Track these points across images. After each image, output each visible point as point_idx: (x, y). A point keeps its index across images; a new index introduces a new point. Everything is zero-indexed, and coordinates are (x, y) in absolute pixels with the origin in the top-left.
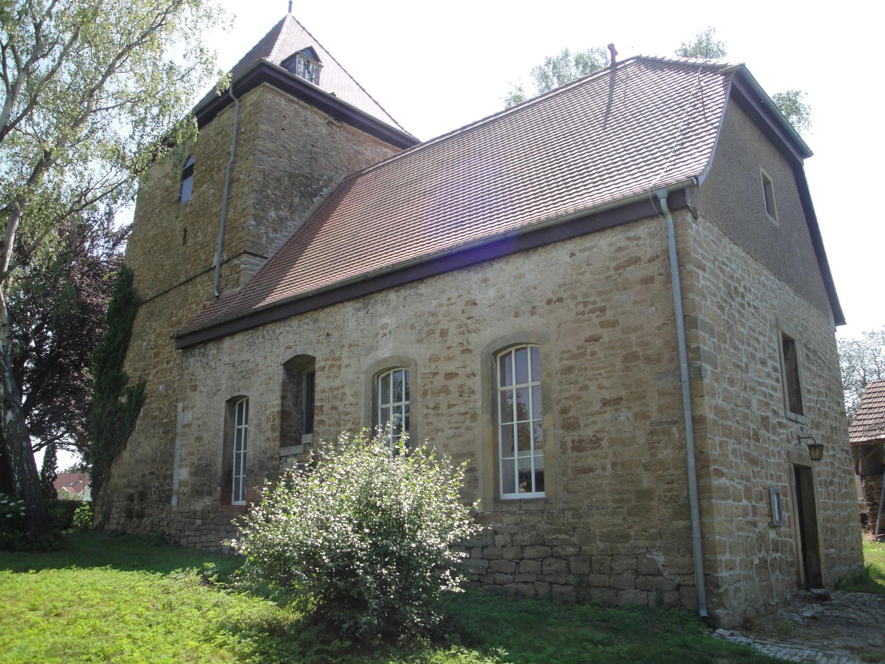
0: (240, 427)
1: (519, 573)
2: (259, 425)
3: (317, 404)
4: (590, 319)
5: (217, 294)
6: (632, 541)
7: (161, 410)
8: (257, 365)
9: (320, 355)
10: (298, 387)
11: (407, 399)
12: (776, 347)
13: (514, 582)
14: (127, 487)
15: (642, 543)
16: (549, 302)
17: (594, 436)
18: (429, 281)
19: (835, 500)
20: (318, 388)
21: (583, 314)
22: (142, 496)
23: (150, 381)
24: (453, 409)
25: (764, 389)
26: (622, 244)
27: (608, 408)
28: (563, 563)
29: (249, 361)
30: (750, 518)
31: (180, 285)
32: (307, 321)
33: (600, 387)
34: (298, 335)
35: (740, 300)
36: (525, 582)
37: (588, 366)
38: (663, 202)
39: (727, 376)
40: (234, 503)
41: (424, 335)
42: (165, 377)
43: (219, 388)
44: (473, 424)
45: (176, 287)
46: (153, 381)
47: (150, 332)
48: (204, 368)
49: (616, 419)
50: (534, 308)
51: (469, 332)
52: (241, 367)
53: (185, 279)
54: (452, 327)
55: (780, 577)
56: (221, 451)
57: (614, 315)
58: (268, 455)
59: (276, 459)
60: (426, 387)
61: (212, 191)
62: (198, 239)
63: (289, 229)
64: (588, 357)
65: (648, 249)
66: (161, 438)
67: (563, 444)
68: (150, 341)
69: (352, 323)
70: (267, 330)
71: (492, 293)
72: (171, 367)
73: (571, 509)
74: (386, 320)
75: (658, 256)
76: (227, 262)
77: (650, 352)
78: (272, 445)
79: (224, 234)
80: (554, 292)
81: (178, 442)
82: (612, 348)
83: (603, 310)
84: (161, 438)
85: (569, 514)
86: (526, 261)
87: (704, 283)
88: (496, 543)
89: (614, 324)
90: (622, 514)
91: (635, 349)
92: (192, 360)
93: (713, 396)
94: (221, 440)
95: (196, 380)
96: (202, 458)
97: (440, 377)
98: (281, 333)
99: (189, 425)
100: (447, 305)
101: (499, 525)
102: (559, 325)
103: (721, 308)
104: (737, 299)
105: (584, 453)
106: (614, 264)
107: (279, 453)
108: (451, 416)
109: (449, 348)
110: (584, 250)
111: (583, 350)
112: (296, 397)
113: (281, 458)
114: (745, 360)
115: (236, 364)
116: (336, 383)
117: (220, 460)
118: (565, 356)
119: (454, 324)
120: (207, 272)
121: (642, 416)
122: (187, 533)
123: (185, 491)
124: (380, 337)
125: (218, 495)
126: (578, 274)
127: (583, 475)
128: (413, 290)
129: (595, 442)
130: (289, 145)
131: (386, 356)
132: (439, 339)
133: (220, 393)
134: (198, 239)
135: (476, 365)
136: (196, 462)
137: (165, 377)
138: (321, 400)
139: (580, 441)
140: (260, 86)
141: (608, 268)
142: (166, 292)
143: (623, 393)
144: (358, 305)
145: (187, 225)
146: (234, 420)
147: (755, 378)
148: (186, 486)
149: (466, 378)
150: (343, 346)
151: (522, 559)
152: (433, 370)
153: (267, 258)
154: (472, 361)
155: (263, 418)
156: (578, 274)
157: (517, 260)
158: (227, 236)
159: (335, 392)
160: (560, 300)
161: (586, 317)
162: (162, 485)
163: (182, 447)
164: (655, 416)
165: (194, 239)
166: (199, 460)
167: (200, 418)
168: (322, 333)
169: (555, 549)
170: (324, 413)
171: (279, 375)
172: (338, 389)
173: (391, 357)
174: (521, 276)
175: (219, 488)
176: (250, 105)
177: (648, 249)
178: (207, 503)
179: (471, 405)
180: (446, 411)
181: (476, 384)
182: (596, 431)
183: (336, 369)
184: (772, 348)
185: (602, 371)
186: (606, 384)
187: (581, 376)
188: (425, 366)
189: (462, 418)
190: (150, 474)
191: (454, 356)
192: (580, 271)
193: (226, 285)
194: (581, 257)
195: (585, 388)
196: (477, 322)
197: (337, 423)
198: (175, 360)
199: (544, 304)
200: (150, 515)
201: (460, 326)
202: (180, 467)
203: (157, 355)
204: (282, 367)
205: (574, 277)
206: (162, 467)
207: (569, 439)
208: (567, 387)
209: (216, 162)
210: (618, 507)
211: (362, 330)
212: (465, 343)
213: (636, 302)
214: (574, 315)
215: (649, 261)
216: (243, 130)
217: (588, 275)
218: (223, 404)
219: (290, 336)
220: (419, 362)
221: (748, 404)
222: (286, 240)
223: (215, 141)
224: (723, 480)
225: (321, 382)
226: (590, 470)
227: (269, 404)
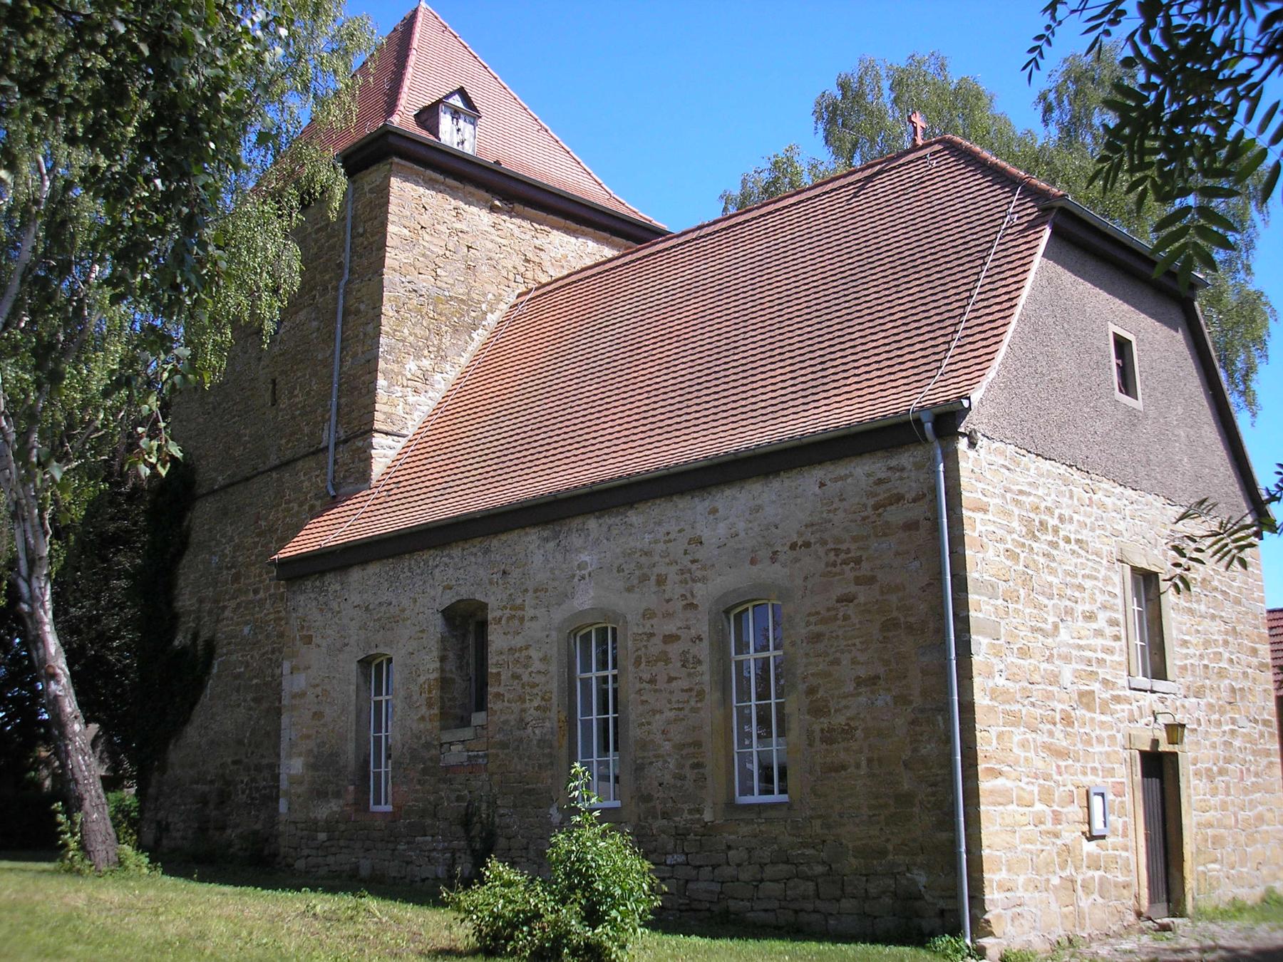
0: (378, 698)
1: (758, 898)
2: (408, 697)
3: (492, 670)
4: (842, 573)
5: (332, 493)
6: (890, 857)
7: (247, 665)
8: (403, 610)
9: (494, 600)
10: (463, 642)
11: (615, 667)
12: (1118, 591)
13: (752, 910)
14: (197, 783)
15: (900, 859)
16: (793, 546)
17: (847, 724)
18: (642, 507)
19: (1228, 794)
20: (492, 648)
21: (834, 565)
22: (224, 798)
23: (227, 619)
24: (674, 684)
25: (1088, 654)
26: (883, 476)
27: (863, 690)
28: (811, 885)
29: (390, 604)
30: (1049, 826)
31: (271, 470)
32: (474, 550)
33: (854, 662)
34: (462, 571)
35: (1050, 538)
36: (766, 911)
37: (840, 633)
38: (928, 426)
39: (1015, 647)
40: (373, 808)
41: (636, 582)
42: (253, 615)
43: (346, 641)
44: (699, 705)
45: (263, 473)
46: (232, 619)
47: (224, 541)
48: (321, 610)
49: (872, 703)
50: (775, 553)
51: (694, 581)
52: (379, 612)
53: (277, 462)
54: (672, 573)
55: (1100, 900)
56: (353, 734)
57: (872, 569)
58: (423, 741)
59: (435, 747)
60: (639, 653)
61: (315, 324)
62: (297, 400)
63: (437, 386)
64: (839, 622)
65: (914, 485)
66: (250, 709)
67: (810, 734)
68: (225, 555)
69: (538, 559)
70: (416, 560)
71: (722, 529)
72: (261, 599)
73: (820, 817)
74: (585, 557)
75: (924, 495)
76: (346, 441)
77: (912, 620)
78: (429, 726)
79: (339, 397)
80: (800, 534)
81: (285, 720)
82: (869, 612)
83: (858, 561)
84: (250, 709)
85: (817, 823)
86: (766, 489)
87: (983, 529)
88: (730, 860)
89: (871, 580)
90: (878, 823)
91: (895, 614)
92: (302, 598)
93: (990, 675)
94: (353, 717)
95: (309, 628)
96: (324, 743)
97: (657, 640)
98: (437, 566)
99: (303, 694)
100: (665, 542)
101: (732, 837)
102: (806, 578)
103: (1015, 557)
104: (1043, 537)
105: (835, 746)
106: (871, 502)
107: (439, 739)
108: (671, 692)
109: (668, 601)
110: (836, 480)
111: (833, 613)
112: (461, 657)
113: (441, 745)
114: (1051, 619)
115: (371, 607)
116: (518, 642)
117: (351, 747)
118: (812, 619)
119: (675, 568)
120: (313, 453)
121: (901, 700)
122: (306, 852)
123: (299, 791)
124: (576, 580)
125: (350, 798)
126: (829, 511)
127: (833, 774)
128: (620, 517)
129: (847, 732)
130: (432, 252)
131: (587, 607)
132: (654, 589)
133: (347, 649)
134: (297, 400)
135: (702, 627)
136: (315, 750)
137: (253, 615)
138: (497, 664)
139: (831, 730)
140: (385, 162)
141: (865, 506)
142: (247, 479)
143: (881, 670)
144: (546, 534)
145: (277, 373)
146: (370, 689)
147: (1071, 641)
148: (301, 783)
149: (690, 643)
150: (526, 590)
151: (762, 881)
152: (648, 629)
153: (404, 436)
154: (698, 620)
155: (415, 688)
156: (829, 511)
157: (754, 486)
158: (343, 400)
159: (517, 655)
160: (807, 545)
161: (838, 569)
162: (253, 780)
163: (292, 726)
164: (917, 701)
165: (289, 399)
166: (319, 746)
167: (318, 685)
168: (495, 570)
169: (801, 868)
170: (502, 684)
171: (437, 626)
172: (521, 649)
173: (592, 609)
174: (758, 509)
175: (351, 788)
176: (371, 191)
177: (914, 485)
178: (335, 809)
179: (697, 679)
180: (665, 686)
181: (703, 651)
182: (848, 719)
183: (516, 622)
184: (1110, 592)
185: (857, 641)
186: (862, 658)
187: (832, 646)
188: (638, 625)
189: (685, 696)
190: (234, 763)
191: (674, 612)
192: (832, 508)
193: (345, 477)
194: (833, 488)
195: (836, 662)
196: (704, 568)
197: (520, 697)
198: (267, 588)
199: (786, 548)
200: (237, 826)
201: (682, 572)
202: (290, 756)
203: (236, 578)
204: (439, 615)
205: (825, 515)
206: (252, 753)
207: (817, 727)
208: (813, 660)
209: (318, 276)
210: (874, 815)
211: (552, 570)
212: (688, 595)
213: (897, 554)
214: (823, 566)
215: (914, 501)
216: (361, 230)
217: (841, 514)
218: (354, 666)
219: (451, 571)
220: (629, 618)
221: (1054, 679)
222: (433, 404)
223: (316, 241)
224: (1000, 782)
225: (497, 640)
226: (843, 767)
227: (421, 669)
